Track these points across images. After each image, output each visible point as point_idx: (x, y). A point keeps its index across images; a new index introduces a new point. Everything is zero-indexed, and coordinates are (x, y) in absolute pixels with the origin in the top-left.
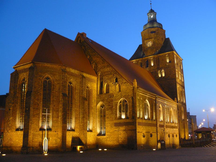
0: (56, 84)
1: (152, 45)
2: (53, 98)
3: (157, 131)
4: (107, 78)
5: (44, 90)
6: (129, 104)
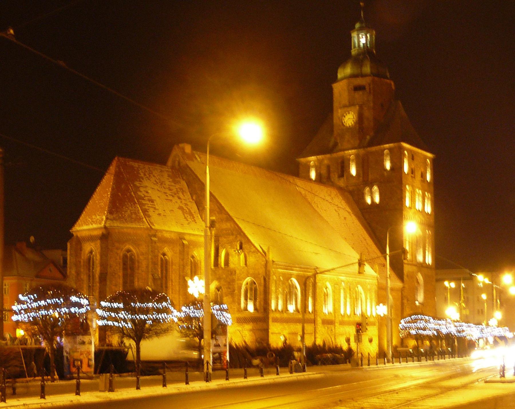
2: (138, 281)
3: (315, 331)
5: (125, 269)
6: (260, 289)
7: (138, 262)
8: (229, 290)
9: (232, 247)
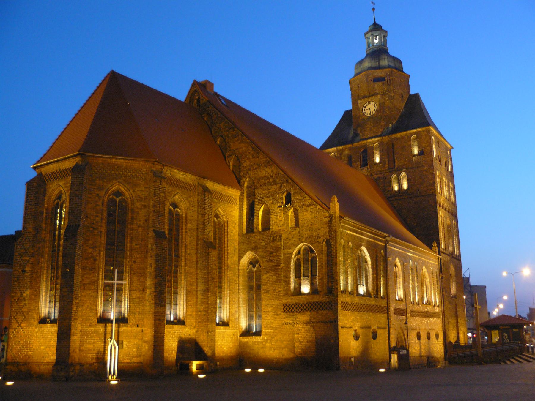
0: (139, 207)
1: (378, 111)
2: (131, 242)
3: (388, 325)
4: (264, 192)
6: (320, 259)
7: (133, 211)
8: (271, 264)
9: (275, 201)
